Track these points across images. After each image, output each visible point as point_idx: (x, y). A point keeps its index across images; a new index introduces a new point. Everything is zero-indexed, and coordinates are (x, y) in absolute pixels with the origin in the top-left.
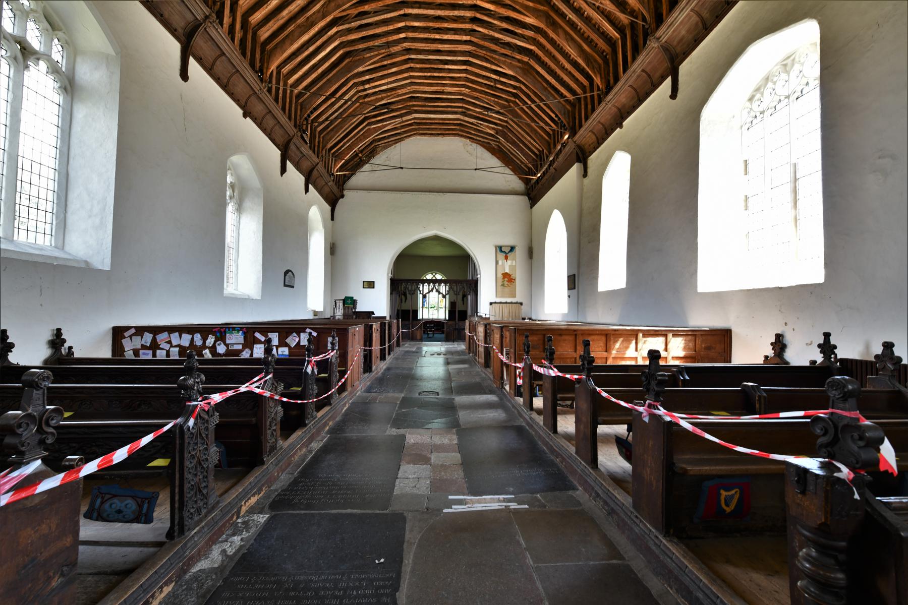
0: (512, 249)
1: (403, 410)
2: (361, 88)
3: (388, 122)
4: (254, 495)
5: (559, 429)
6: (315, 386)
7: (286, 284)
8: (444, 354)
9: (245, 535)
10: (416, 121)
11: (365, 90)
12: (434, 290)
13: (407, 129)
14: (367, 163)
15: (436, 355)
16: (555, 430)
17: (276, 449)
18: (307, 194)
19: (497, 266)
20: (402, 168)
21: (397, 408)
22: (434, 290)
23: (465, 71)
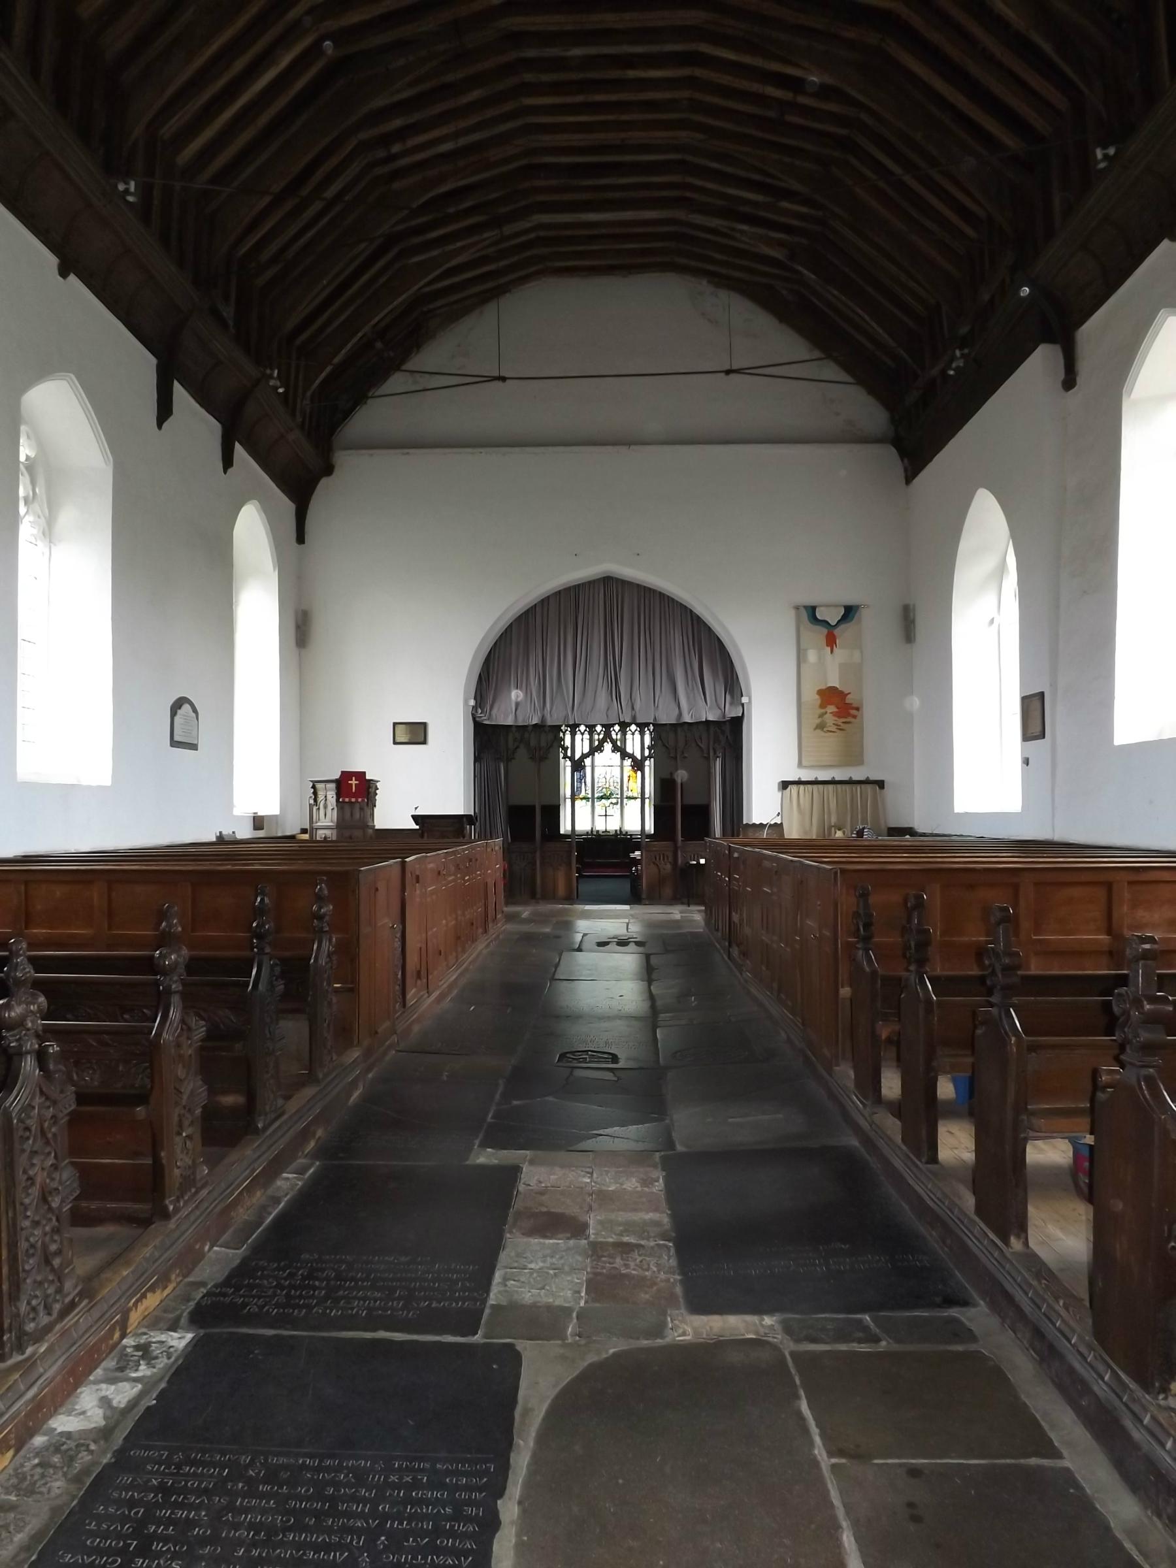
0: (850, 612)
1: (515, 1103)
2: (381, 154)
3: (459, 244)
4: (152, 1289)
7: (177, 738)
8: (638, 944)
9: (144, 1370)
10: (542, 233)
11: (392, 158)
12: (608, 746)
13: (516, 258)
14: (398, 368)
15: (613, 947)
18: (230, 470)
20: (503, 379)
21: (497, 1097)
22: (608, 746)
23: (691, 82)
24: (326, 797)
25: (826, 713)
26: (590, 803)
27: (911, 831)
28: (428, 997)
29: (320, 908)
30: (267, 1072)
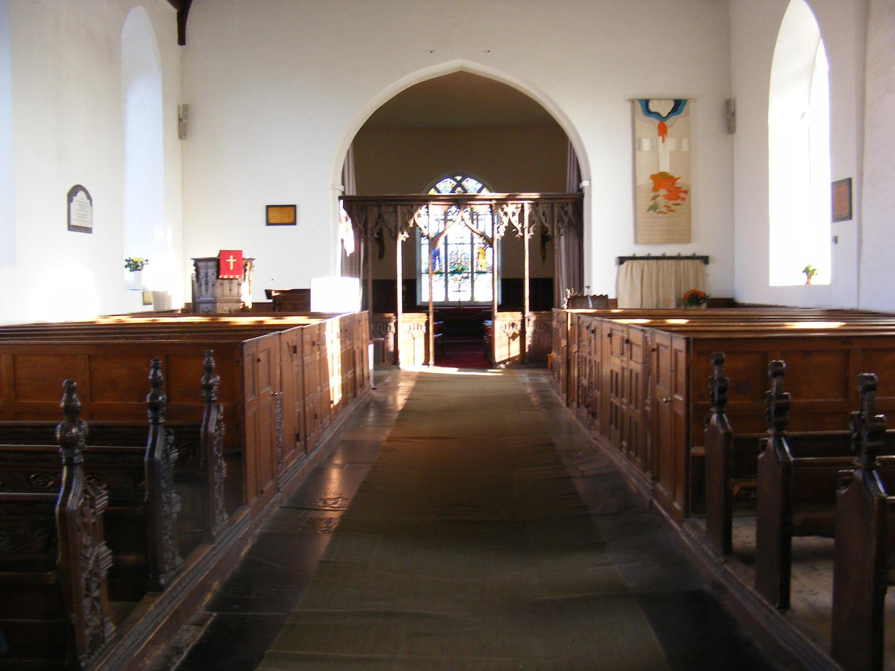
0: (678, 105)
5: (796, 600)
6: (174, 495)
16: (784, 603)
17: (104, 643)
19: (638, 153)
24: (207, 274)
25: (658, 196)
26: (443, 277)
27: (730, 303)
28: (307, 457)
29: (208, 379)
30: (166, 534)
